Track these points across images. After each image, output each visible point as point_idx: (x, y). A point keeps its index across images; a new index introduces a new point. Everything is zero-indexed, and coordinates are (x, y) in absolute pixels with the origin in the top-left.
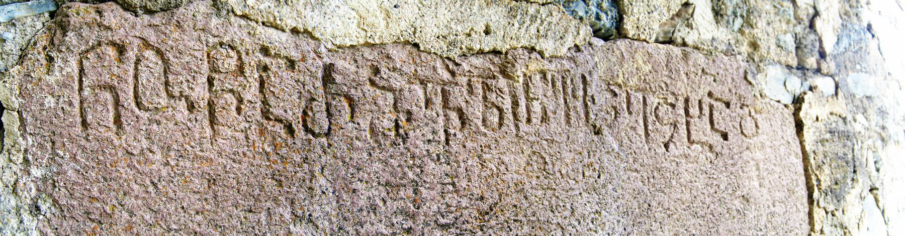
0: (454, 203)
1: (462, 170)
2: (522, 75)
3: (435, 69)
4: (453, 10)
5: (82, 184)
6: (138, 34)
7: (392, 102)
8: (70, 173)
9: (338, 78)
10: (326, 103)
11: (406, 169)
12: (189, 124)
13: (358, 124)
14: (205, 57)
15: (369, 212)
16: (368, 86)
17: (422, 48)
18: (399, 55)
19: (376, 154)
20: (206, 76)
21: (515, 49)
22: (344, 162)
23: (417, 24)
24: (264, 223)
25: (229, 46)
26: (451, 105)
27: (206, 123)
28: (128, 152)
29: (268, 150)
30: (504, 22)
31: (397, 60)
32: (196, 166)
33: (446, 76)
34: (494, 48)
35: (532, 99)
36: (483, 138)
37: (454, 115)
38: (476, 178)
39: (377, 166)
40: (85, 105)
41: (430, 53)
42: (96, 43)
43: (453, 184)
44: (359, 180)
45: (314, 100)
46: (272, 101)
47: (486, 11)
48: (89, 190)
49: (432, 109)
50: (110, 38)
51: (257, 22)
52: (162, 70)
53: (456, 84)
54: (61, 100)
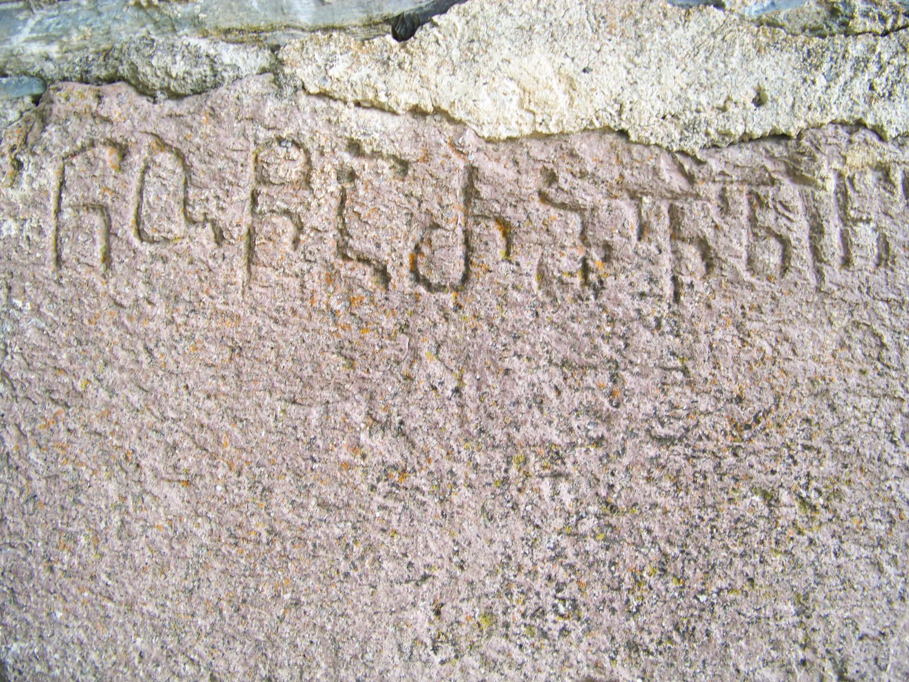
0: (685, 403)
1: (702, 346)
2: (832, 176)
3: (656, 171)
4: (691, 68)
5: (45, 349)
6: (150, 129)
7: (578, 228)
8: (30, 332)
9: (485, 191)
10: (465, 232)
11: (598, 341)
12: (211, 262)
13: (518, 264)
14: (251, 161)
15: (530, 407)
16: (536, 203)
17: (633, 138)
18: (592, 151)
19: (548, 313)
20: (249, 189)
21: (819, 127)
22: (491, 325)
23: (625, 98)
24: (314, 422)
25: (293, 142)
26: (685, 233)
27: (240, 262)
28: (116, 303)
29: (337, 307)
30: (792, 79)
31: (588, 159)
32: (214, 325)
33: (678, 183)
34: (774, 129)
35: (855, 221)
36: (746, 292)
37: (691, 253)
38: (730, 363)
39: (547, 333)
40: (61, 233)
41: (648, 145)
42: (87, 142)
43: (685, 371)
44: (515, 354)
45: (437, 226)
46: (355, 228)
47: (756, 62)
48: (55, 358)
49: (650, 241)
50: (109, 135)
51: (345, 103)
52: (182, 181)
53: (697, 196)
54: (27, 226)
